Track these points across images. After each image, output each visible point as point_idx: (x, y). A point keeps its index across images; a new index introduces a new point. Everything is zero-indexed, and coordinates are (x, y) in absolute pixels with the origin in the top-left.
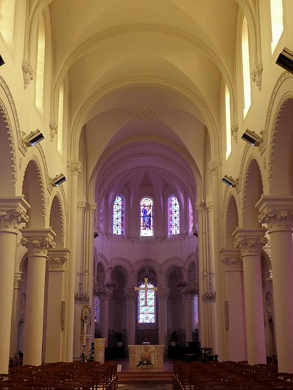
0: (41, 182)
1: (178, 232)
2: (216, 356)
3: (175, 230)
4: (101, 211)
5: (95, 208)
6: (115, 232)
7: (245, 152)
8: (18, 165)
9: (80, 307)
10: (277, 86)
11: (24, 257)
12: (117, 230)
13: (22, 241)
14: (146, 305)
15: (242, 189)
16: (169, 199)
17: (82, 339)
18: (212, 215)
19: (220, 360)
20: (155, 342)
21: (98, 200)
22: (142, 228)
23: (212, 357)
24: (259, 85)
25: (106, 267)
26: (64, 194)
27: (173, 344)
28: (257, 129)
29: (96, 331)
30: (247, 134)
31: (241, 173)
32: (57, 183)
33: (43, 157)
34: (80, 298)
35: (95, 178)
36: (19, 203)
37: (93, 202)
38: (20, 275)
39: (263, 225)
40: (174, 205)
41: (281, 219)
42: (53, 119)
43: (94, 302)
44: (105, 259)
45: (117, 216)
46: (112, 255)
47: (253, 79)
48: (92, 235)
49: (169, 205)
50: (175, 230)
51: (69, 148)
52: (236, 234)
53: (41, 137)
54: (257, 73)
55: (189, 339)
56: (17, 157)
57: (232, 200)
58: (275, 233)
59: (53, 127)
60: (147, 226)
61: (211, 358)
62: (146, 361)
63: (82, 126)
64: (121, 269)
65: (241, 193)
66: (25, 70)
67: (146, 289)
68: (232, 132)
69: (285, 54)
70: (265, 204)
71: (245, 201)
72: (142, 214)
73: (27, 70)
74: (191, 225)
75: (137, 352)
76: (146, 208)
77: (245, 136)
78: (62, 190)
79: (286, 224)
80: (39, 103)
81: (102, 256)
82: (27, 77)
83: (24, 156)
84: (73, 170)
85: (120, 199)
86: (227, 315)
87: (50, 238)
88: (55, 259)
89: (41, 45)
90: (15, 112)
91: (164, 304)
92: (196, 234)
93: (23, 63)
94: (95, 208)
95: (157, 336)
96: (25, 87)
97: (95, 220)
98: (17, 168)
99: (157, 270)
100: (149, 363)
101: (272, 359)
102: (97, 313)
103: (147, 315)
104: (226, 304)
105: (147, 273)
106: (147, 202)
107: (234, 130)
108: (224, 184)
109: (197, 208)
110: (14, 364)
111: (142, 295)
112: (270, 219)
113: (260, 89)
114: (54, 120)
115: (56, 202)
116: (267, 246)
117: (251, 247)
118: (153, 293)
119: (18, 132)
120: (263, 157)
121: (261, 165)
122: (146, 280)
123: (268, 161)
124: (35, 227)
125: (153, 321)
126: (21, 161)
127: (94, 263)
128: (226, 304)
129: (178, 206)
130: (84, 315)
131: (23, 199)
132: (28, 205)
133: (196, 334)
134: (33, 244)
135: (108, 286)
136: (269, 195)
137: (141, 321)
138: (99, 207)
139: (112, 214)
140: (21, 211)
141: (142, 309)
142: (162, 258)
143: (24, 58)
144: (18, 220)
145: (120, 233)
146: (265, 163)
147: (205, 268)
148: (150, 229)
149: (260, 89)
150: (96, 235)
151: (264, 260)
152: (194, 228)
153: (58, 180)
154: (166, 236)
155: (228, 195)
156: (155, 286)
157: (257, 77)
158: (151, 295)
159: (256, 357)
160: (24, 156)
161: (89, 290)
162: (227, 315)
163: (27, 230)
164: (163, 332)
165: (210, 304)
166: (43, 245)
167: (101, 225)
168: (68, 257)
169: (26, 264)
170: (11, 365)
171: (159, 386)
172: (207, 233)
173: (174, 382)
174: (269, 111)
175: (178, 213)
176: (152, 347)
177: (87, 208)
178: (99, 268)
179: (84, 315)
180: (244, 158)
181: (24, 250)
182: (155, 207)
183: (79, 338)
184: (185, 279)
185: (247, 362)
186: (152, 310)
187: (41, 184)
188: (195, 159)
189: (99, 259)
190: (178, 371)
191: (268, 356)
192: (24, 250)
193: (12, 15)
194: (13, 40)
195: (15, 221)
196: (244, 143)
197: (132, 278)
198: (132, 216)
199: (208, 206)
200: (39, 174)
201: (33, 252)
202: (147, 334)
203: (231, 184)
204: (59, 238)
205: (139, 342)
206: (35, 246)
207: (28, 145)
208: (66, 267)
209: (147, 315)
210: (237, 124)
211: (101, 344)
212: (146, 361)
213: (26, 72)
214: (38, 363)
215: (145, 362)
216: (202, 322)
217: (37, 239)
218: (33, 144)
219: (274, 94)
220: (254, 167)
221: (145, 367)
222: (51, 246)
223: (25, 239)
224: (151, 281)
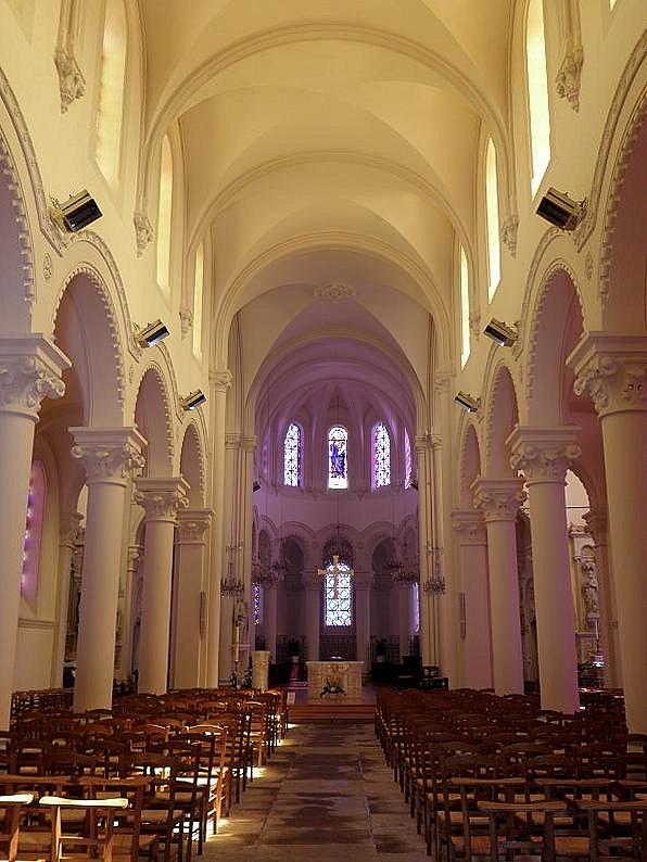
0: (165, 404)
1: (388, 482)
2: (446, 680)
3: (382, 478)
4: (265, 448)
5: (254, 444)
6: (287, 482)
7: (491, 356)
8: (127, 376)
9: (230, 600)
10: (541, 250)
11: (140, 525)
12: (291, 479)
13: (137, 497)
14: (335, 597)
15: (526, 346)
16: (373, 430)
17: (233, 650)
18: (439, 454)
19: (451, 687)
20: (350, 656)
21: (260, 429)
22: (331, 475)
23: (441, 681)
24: (573, 96)
25: (273, 537)
26: (203, 423)
27: (380, 659)
28: (575, 191)
29: (257, 639)
30: (493, 326)
31: (485, 388)
32: (191, 405)
33: (169, 364)
34: (229, 587)
35: (255, 395)
36: (38, 349)
37: (251, 433)
38: (135, 550)
39: (520, 472)
40: (382, 439)
41: (547, 464)
42: (141, 208)
43: (253, 593)
44: (273, 527)
45: (291, 456)
46: (284, 517)
47: (503, 239)
48: (250, 487)
49: (373, 439)
50: (382, 478)
51: (212, 347)
52: (476, 487)
53: (164, 331)
54: (509, 229)
55: (405, 652)
56: (125, 365)
57: (504, 377)
58: (614, 416)
59: (186, 317)
60: (339, 473)
61: (439, 684)
62: (334, 687)
63: (233, 313)
64: (298, 542)
65: (485, 422)
66: (139, 226)
67: (337, 572)
68: (471, 323)
69: (551, 198)
70: (593, 350)
71: (532, 369)
72: (331, 454)
73: (143, 227)
74: (408, 472)
75: (321, 670)
76: (337, 443)
77: (489, 330)
78: (201, 416)
79: (642, 396)
80: (162, 278)
81: (266, 519)
82: (66, 85)
83: (61, 256)
84: (217, 384)
85: (296, 428)
86: (463, 611)
87: (180, 493)
88: (190, 525)
89: (114, 48)
90: (121, 293)
91: (367, 596)
92: (415, 486)
93: (57, 51)
94: (254, 444)
95: (354, 646)
96: (62, 107)
97: (255, 463)
98: (126, 381)
99: (354, 543)
100: (339, 690)
101: (532, 687)
102: (257, 610)
103: (338, 612)
104: (462, 597)
105: (339, 547)
106: (338, 435)
107: (474, 320)
108: (459, 406)
109: (416, 444)
110: (127, 689)
111: (330, 583)
112: (528, 463)
113: (514, 255)
114: (144, 210)
115: (191, 434)
116: (526, 504)
117: (500, 507)
118: (348, 579)
119: (127, 324)
120: (519, 362)
121: (478, 429)
122: (336, 558)
123: (526, 370)
124: (156, 473)
125: (349, 623)
126: (132, 370)
127: (254, 531)
128: (462, 597)
129: (387, 440)
130: (237, 613)
131: (134, 430)
132: (66, 359)
133: (416, 644)
134: (155, 502)
135: (276, 567)
136: (600, 329)
137: (329, 623)
138: (262, 441)
139: (283, 453)
140: (132, 450)
141: (331, 605)
142: (361, 521)
143: (137, 208)
144: (127, 465)
145: (295, 483)
146: (482, 430)
147: (429, 539)
148: (343, 477)
149: (514, 255)
150: (256, 487)
151: (522, 526)
152: (413, 476)
153: (195, 399)
154: (367, 490)
155: (494, 365)
156: (351, 567)
157: (509, 236)
158: (345, 581)
159: (508, 685)
160: (61, 256)
161: (245, 576)
162: (463, 611)
163: (144, 479)
164: (364, 643)
165: (438, 599)
166: (170, 502)
167: (265, 471)
168: (210, 523)
169: (143, 533)
170: (116, 695)
171: (354, 727)
172: (433, 484)
173: (376, 721)
174: (529, 291)
175: (388, 450)
176: (345, 665)
177: (241, 444)
178: (262, 538)
179: (237, 613)
180: (489, 365)
181: (140, 511)
182: (351, 442)
183: (226, 650)
184: (399, 557)
185: (493, 690)
186: (347, 604)
187: (111, 325)
188: (411, 361)
189: (261, 525)
190: (382, 703)
191: (529, 679)
192: (140, 511)
193: (118, 139)
194: (120, 177)
195: (122, 465)
196: (489, 340)
197: (313, 555)
198: (314, 457)
199: (434, 440)
200: (108, 311)
201: (97, 475)
202: (338, 644)
203: (469, 407)
204: (195, 490)
205: (324, 657)
206: (157, 505)
207: (144, 345)
208: (207, 535)
209: (338, 612)
210: (517, 216)
211: (263, 659)
212: (334, 687)
213: (141, 229)
214: (161, 689)
215: (333, 689)
216: (425, 628)
217: (158, 495)
218: (151, 344)
219: (536, 262)
220: (504, 377)
221: (333, 696)
222: (181, 505)
223: (141, 494)
224: (343, 559)
